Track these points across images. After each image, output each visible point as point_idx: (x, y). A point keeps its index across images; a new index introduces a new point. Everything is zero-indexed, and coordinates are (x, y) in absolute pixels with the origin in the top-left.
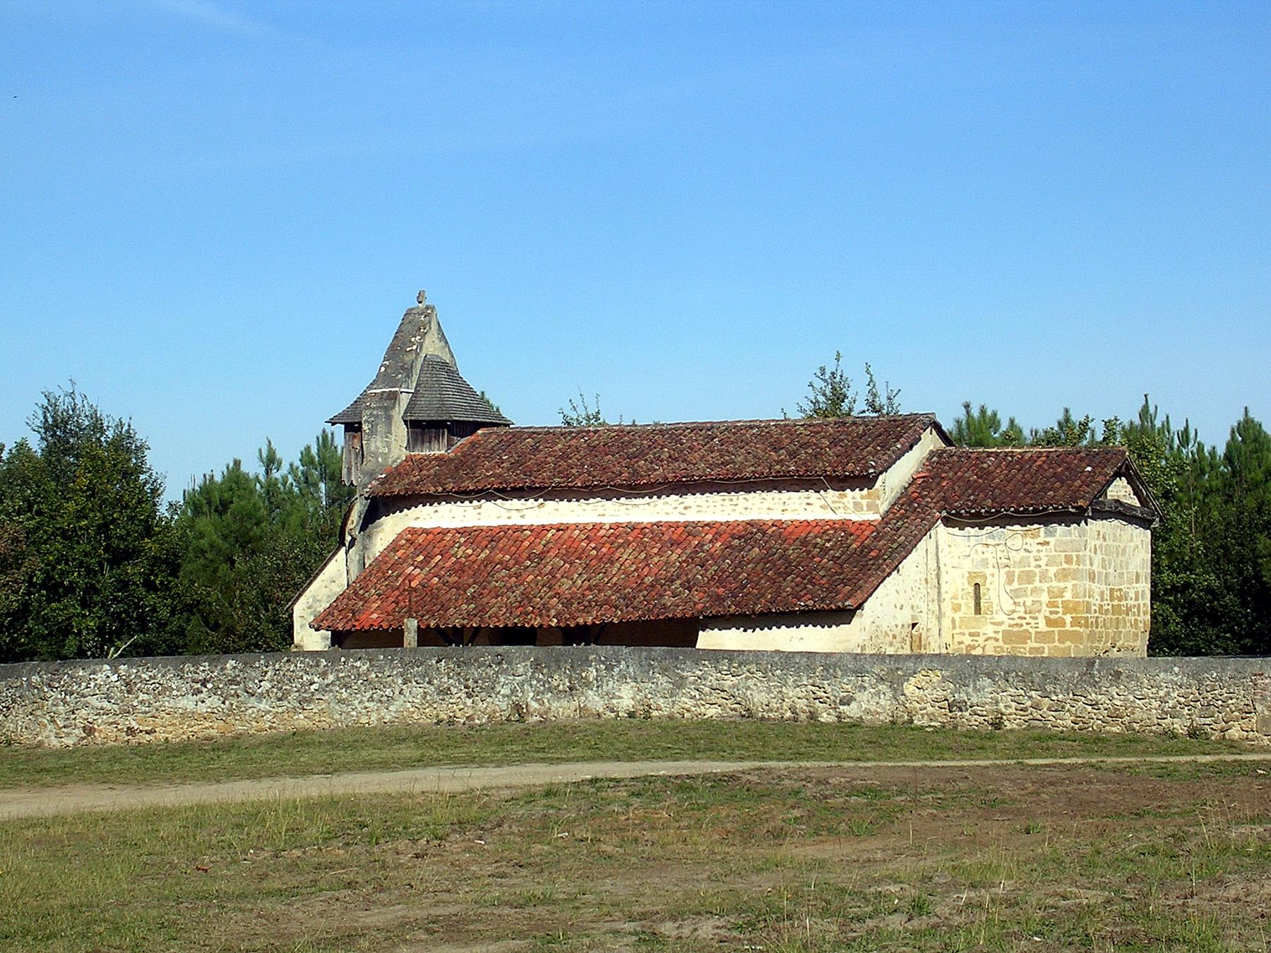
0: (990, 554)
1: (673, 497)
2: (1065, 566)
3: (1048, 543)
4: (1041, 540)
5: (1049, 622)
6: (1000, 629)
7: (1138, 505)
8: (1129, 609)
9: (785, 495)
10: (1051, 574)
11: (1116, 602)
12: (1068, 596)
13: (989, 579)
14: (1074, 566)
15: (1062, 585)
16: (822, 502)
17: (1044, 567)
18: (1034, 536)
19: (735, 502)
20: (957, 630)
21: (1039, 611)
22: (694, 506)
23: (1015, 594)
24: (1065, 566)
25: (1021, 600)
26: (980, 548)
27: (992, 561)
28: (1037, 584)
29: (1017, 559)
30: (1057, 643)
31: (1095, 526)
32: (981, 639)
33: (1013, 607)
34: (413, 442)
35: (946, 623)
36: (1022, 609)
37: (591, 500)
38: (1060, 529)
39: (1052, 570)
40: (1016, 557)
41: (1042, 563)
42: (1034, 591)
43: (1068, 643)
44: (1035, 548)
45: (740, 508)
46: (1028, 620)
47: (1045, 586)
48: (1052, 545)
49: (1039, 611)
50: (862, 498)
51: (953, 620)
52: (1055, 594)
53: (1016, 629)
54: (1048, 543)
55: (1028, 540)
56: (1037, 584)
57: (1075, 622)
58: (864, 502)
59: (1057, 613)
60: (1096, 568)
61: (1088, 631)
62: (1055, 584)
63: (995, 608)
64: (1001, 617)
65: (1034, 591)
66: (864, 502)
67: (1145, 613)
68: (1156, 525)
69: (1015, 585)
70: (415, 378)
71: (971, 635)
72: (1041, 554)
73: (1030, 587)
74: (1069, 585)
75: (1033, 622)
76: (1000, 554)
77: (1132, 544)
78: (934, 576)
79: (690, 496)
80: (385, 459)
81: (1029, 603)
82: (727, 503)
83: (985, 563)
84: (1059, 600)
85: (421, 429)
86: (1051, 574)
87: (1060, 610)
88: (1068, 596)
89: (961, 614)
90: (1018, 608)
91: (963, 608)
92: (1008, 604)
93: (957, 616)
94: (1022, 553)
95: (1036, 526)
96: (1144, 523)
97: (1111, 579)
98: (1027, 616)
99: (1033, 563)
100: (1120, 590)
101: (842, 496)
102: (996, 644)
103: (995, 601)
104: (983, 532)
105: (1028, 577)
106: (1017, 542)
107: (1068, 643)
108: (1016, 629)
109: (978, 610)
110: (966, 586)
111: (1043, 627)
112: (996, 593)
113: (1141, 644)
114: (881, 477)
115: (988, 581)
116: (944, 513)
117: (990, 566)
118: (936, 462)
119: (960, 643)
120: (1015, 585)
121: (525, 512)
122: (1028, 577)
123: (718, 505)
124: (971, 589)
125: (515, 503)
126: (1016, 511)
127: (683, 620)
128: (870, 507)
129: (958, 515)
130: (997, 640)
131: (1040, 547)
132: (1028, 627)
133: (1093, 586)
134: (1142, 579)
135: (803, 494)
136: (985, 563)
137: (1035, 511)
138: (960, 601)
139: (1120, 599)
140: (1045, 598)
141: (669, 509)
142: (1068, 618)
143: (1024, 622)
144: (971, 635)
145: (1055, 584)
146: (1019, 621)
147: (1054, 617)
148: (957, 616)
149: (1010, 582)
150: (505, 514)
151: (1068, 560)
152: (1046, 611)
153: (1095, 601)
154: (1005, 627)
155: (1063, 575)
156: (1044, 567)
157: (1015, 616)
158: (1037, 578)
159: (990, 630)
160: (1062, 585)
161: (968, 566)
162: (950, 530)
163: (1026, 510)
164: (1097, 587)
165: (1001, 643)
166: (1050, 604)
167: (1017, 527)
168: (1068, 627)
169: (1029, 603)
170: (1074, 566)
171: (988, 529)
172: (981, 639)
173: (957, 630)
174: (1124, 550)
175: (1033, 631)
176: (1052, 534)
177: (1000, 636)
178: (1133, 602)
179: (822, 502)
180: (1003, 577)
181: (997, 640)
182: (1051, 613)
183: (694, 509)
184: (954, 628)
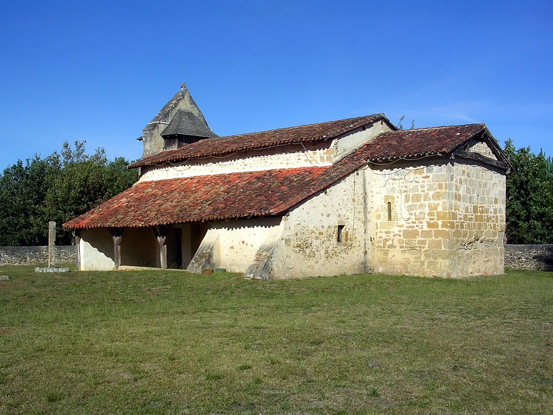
0: (396, 184)
1: (240, 160)
2: (438, 190)
3: (428, 177)
4: (424, 175)
5: (429, 225)
6: (402, 229)
7: (496, 159)
8: (489, 219)
9: (289, 155)
10: (430, 196)
11: (453, 211)
12: (440, 209)
13: (396, 199)
14: (444, 191)
15: (437, 202)
16: (305, 158)
17: (426, 192)
18: (421, 173)
19: (266, 161)
20: (379, 230)
21: (424, 218)
22: (248, 164)
23: (410, 208)
24: (438, 190)
25: (413, 212)
26: (391, 181)
27: (397, 189)
28: (422, 202)
29: (411, 187)
30: (433, 238)
31: (459, 168)
32: (391, 235)
33: (408, 216)
34: (167, 145)
35: (371, 226)
36: (414, 217)
37: (209, 164)
38: (435, 168)
39: (431, 193)
40: (411, 186)
41: (425, 189)
42: (421, 206)
43: (440, 238)
44: (421, 180)
45: (268, 164)
46: (417, 224)
47: (427, 203)
48: (431, 178)
49: (424, 218)
50: (324, 154)
51: (377, 225)
52: (433, 208)
53: (410, 229)
54: (428, 177)
55: (417, 175)
56: (422, 202)
57: (444, 225)
58: (325, 156)
59: (434, 219)
60: (461, 192)
61: (454, 231)
62: (432, 202)
63: (399, 217)
64: (402, 222)
65: (421, 206)
66: (325, 156)
67: (501, 221)
68: (508, 172)
69: (410, 203)
70: (170, 119)
71: (386, 233)
72: (425, 184)
73: (418, 204)
74: (441, 202)
75: (420, 225)
76: (402, 185)
77: (492, 182)
78: (361, 197)
79: (247, 159)
80: (149, 153)
81: (418, 214)
82: (263, 161)
83: (393, 190)
84: (435, 211)
85: (169, 138)
86: (430, 196)
87: (436, 217)
88: (440, 209)
89: (381, 220)
90: (411, 217)
91: (382, 217)
92: (406, 215)
93: (379, 222)
94: (414, 184)
95: (422, 167)
96: (500, 170)
97: (475, 200)
98: (417, 221)
99: (420, 189)
100: (482, 207)
101: (314, 154)
102: (400, 238)
103: (399, 212)
104: (393, 172)
105: (417, 198)
106: (419, 177)
107: (440, 238)
108: (410, 229)
109: (390, 218)
110: (384, 204)
111: (426, 228)
112: (401, 209)
113: (183, 230)
114: (334, 142)
115: (395, 200)
116: (368, 161)
117: (396, 192)
118: (381, 138)
119: (380, 237)
120: (410, 203)
121: (183, 172)
122: (417, 198)
123: (259, 162)
124: (386, 206)
125: (181, 168)
126: (408, 157)
127: (199, 222)
128: (328, 159)
129: (376, 161)
130: (400, 236)
131: (424, 179)
132: (416, 228)
133: (459, 203)
134: (500, 201)
135: (297, 154)
136: (393, 190)
137: (419, 156)
138: (380, 213)
139: (482, 212)
140: (427, 210)
141: (238, 166)
142: (440, 223)
143: (415, 225)
144: (386, 233)
145: (432, 202)
146: (412, 225)
147: (432, 222)
148: (379, 222)
149: (407, 200)
150: (176, 173)
151: (440, 187)
152: (427, 218)
153: (461, 213)
154: (404, 228)
155: (437, 196)
156: (426, 192)
157: (410, 221)
158: (423, 198)
159: (396, 230)
160: (437, 202)
161: (384, 192)
162: (375, 171)
163: (413, 156)
164: (462, 205)
165: (402, 238)
166: (430, 214)
167: (411, 168)
168: (440, 228)
169: (418, 214)
170: (444, 191)
171: (396, 170)
172: (391, 235)
173: (379, 230)
174: (485, 185)
175: (420, 230)
176: (430, 171)
177: (402, 233)
178: (492, 215)
179: (305, 158)
180: (404, 198)
181: (400, 236)
182: (430, 219)
183: (249, 165)
184: (377, 229)
